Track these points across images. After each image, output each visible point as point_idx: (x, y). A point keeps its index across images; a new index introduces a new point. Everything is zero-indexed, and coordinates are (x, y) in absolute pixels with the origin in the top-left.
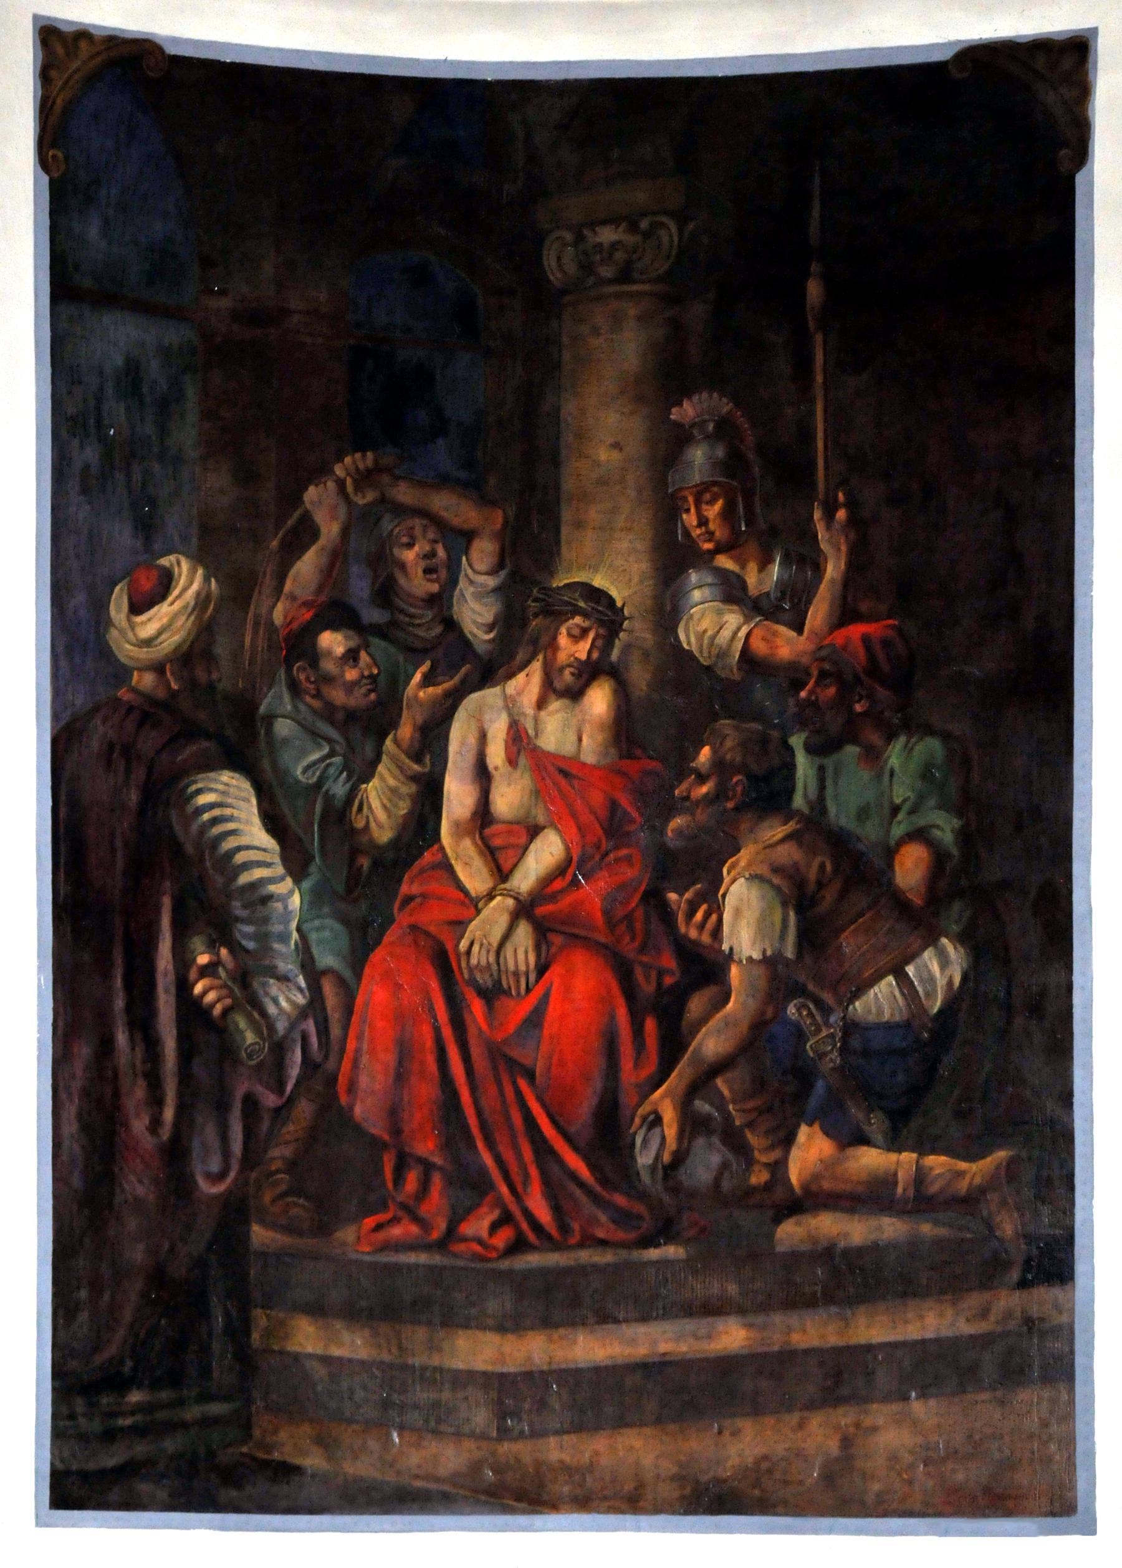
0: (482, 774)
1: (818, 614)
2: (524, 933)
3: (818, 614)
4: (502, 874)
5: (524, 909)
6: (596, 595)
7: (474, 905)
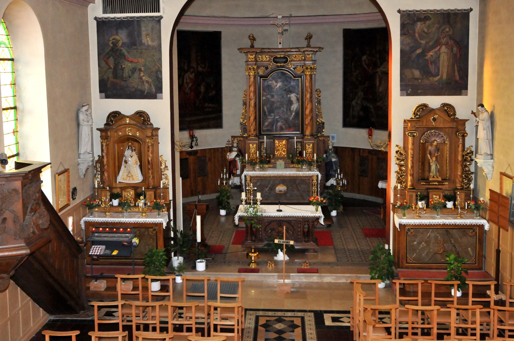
1: (206, 68)
2: (189, 90)
3: (206, 68)
6: (193, 67)
7: (186, 88)
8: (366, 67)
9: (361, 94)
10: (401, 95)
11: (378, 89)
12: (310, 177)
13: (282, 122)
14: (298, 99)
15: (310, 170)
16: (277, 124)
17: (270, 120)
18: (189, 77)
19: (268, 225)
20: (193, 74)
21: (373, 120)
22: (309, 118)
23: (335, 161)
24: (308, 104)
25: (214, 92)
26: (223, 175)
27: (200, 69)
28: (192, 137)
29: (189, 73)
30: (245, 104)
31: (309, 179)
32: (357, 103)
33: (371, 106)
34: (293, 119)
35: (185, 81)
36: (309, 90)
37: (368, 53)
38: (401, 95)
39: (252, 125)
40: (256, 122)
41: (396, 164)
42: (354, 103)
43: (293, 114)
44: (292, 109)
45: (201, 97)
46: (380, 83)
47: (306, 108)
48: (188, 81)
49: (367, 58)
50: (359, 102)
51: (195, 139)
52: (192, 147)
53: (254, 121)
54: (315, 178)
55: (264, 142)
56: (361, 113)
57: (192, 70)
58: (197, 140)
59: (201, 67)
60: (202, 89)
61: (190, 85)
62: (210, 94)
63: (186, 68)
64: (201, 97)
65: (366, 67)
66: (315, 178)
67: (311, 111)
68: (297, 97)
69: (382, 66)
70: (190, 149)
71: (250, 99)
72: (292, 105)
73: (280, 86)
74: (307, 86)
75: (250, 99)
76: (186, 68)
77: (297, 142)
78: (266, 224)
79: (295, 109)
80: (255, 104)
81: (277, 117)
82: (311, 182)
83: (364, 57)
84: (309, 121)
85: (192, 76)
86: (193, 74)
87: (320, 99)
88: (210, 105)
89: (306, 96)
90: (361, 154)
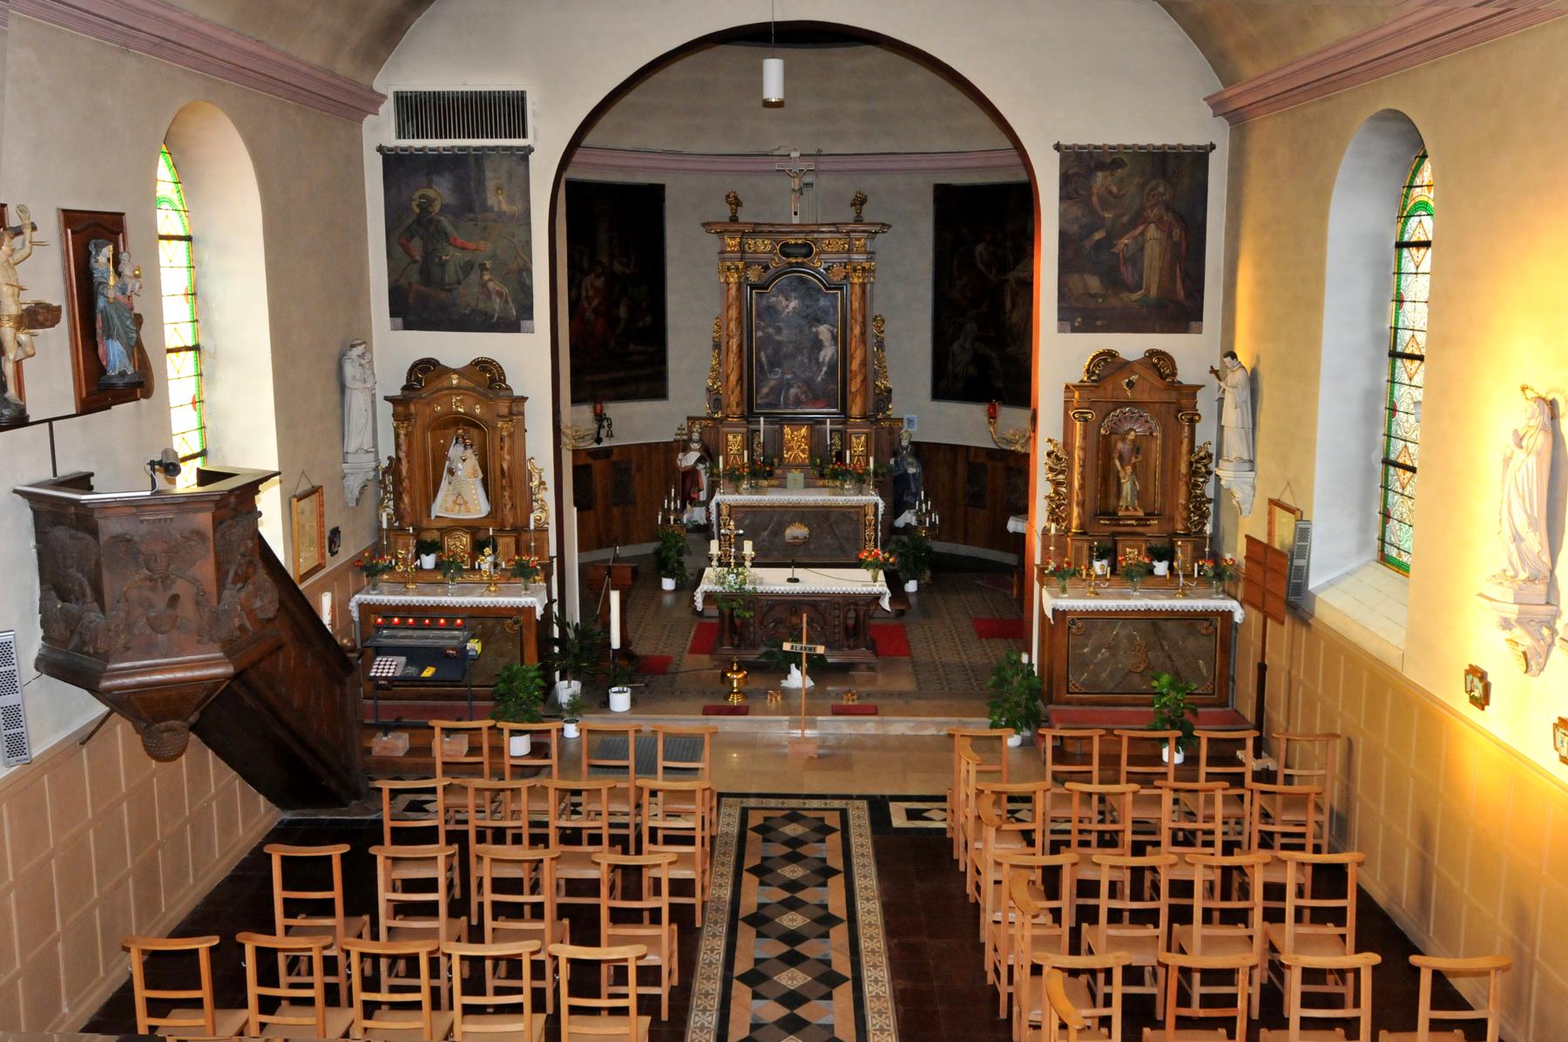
0: (587, 291)
4: (590, 304)
5: (594, 310)
8: (983, 268)
9: (971, 327)
10: (1060, 331)
11: (1010, 318)
12: (859, 507)
13: (799, 387)
14: (834, 338)
15: (861, 492)
16: (788, 390)
17: (772, 383)
18: (592, 285)
19: (769, 611)
20: (602, 279)
21: (999, 384)
22: (859, 378)
23: (913, 474)
24: (856, 349)
25: (648, 320)
26: (669, 503)
27: (617, 267)
28: (600, 418)
29: (592, 276)
30: (717, 346)
31: (858, 513)
32: (963, 347)
33: (993, 355)
34: (822, 380)
35: (584, 293)
36: (859, 318)
37: (988, 237)
38: (1060, 331)
39: (732, 393)
40: (742, 386)
41: (1048, 479)
42: (956, 346)
43: (825, 369)
44: (821, 360)
45: (619, 331)
46: (1014, 305)
47: (852, 357)
48: (591, 293)
49: (985, 249)
50: (967, 345)
51: (605, 423)
52: (599, 440)
53: (737, 383)
54: (870, 511)
55: (759, 431)
56: (972, 370)
57: (599, 270)
58: (610, 425)
59: (620, 263)
60: (623, 312)
61: (595, 303)
62: (641, 324)
63: (586, 265)
64: (619, 331)
65: (983, 268)
66: (870, 511)
67: (864, 364)
68: (832, 332)
69: (1019, 267)
70: (595, 446)
71: (728, 335)
72: (820, 350)
73: (794, 308)
74: (854, 307)
75: (728, 335)
76: (586, 265)
77: (831, 431)
78: (765, 609)
79: (827, 359)
80: (740, 346)
81: (789, 377)
82: (862, 520)
83: (980, 248)
84: (858, 386)
85: (600, 283)
86: (602, 279)
87: (883, 338)
88: (640, 348)
89: (852, 329)
90: (971, 460)
